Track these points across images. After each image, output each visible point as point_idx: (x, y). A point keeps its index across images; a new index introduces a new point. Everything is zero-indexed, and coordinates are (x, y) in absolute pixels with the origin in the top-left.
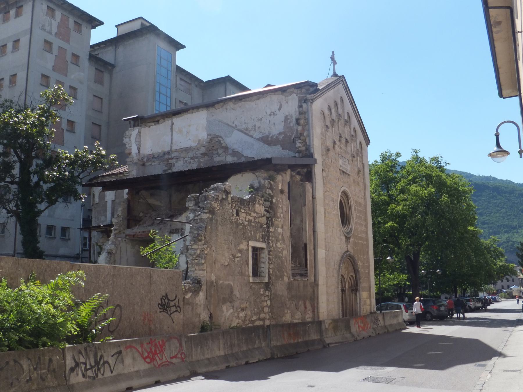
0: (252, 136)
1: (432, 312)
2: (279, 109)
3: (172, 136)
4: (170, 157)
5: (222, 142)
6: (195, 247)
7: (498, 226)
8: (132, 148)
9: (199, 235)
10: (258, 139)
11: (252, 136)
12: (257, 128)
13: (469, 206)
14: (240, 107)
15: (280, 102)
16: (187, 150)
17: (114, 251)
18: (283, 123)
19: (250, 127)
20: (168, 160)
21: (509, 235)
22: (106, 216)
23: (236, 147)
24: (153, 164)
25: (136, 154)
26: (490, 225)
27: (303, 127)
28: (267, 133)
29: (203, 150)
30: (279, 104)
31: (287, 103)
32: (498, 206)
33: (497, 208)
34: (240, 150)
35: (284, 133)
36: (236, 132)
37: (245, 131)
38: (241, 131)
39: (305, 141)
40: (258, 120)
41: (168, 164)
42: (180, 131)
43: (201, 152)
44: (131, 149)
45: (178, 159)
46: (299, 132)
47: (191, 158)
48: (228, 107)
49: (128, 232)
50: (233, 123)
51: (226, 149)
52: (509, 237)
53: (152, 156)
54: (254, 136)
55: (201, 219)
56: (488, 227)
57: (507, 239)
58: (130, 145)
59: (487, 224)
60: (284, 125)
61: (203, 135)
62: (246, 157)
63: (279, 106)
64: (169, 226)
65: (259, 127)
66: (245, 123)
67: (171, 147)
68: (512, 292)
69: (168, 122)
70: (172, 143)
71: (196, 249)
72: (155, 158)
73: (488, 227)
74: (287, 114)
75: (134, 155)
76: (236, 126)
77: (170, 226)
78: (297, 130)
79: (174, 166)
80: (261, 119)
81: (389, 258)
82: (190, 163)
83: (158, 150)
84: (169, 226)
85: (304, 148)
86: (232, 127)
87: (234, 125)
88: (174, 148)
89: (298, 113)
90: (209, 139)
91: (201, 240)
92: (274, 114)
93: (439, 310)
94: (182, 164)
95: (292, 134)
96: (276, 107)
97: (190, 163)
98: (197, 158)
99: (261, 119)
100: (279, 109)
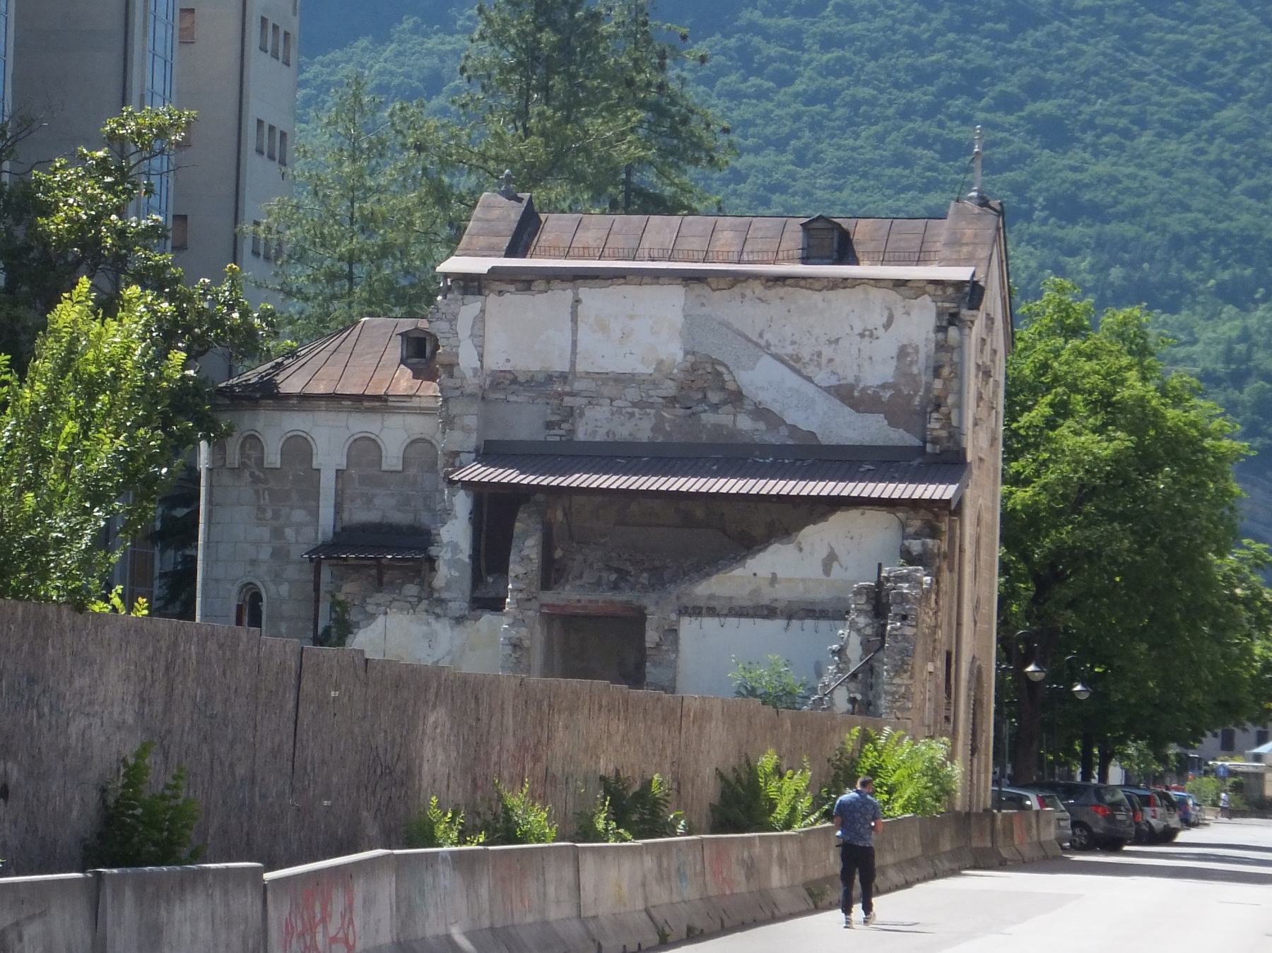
0: (809, 379)
1: (1090, 823)
2: (887, 326)
3: (575, 331)
4: (567, 389)
5: (727, 377)
6: (897, 681)
7: (1177, 242)
8: (461, 351)
9: (904, 662)
10: (828, 389)
11: (809, 379)
12: (824, 361)
13: (1225, 492)
14: (781, 298)
15: (889, 309)
16: (623, 380)
17: (526, 643)
18: (894, 363)
19: (806, 355)
20: (560, 396)
21: (1253, 320)
22: (315, 513)
23: (766, 398)
24: (512, 398)
25: (475, 370)
26: (1114, 229)
27: (944, 384)
28: (851, 379)
29: (670, 389)
30: (886, 313)
31: (908, 314)
32: (1197, 79)
33: (1185, 92)
34: (776, 408)
35: (893, 386)
36: (766, 361)
37: (791, 363)
38: (783, 361)
39: (948, 416)
40: (830, 342)
41: (560, 407)
42: (602, 326)
43: (664, 394)
44: (457, 355)
45: (592, 400)
46: (936, 393)
47: (634, 405)
48: (748, 293)
49: (549, 597)
50: (761, 336)
51: (736, 397)
52: (1245, 336)
53: (509, 376)
54: (816, 380)
55: (903, 635)
56: (1100, 244)
57: (1228, 357)
58: (453, 341)
59: (1097, 213)
60: (897, 368)
61: (673, 351)
62: (793, 429)
63: (885, 320)
64: (673, 597)
65: (831, 360)
66: (793, 343)
67: (573, 364)
68: (1259, 776)
69: (564, 295)
70: (574, 352)
71: (900, 686)
72: (521, 384)
73: (1100, 244)
74: (905, 342)
75: (469, 374)
76: (768, 345)
77: (678, 598)
78: (929, 388)
79: (582, 414)
80: (837, 340)
81: (1078, 688)
82: (632, 415)
83: (527, 363)
84: (673, 597)
85: (944, 433)
86: (756, 344)
87: (763, 343)
88: (580, 368)
89: (933, 345)
90: (689, 365)
91: (905, 672)
92: (871, 335)
93: (1111, 819)
94: (608, 415)
95: (916, 394)
96: (877, 319)
97: (632, 415)
98: (652, 405)
99: (837, 340)
100: (887, 326)
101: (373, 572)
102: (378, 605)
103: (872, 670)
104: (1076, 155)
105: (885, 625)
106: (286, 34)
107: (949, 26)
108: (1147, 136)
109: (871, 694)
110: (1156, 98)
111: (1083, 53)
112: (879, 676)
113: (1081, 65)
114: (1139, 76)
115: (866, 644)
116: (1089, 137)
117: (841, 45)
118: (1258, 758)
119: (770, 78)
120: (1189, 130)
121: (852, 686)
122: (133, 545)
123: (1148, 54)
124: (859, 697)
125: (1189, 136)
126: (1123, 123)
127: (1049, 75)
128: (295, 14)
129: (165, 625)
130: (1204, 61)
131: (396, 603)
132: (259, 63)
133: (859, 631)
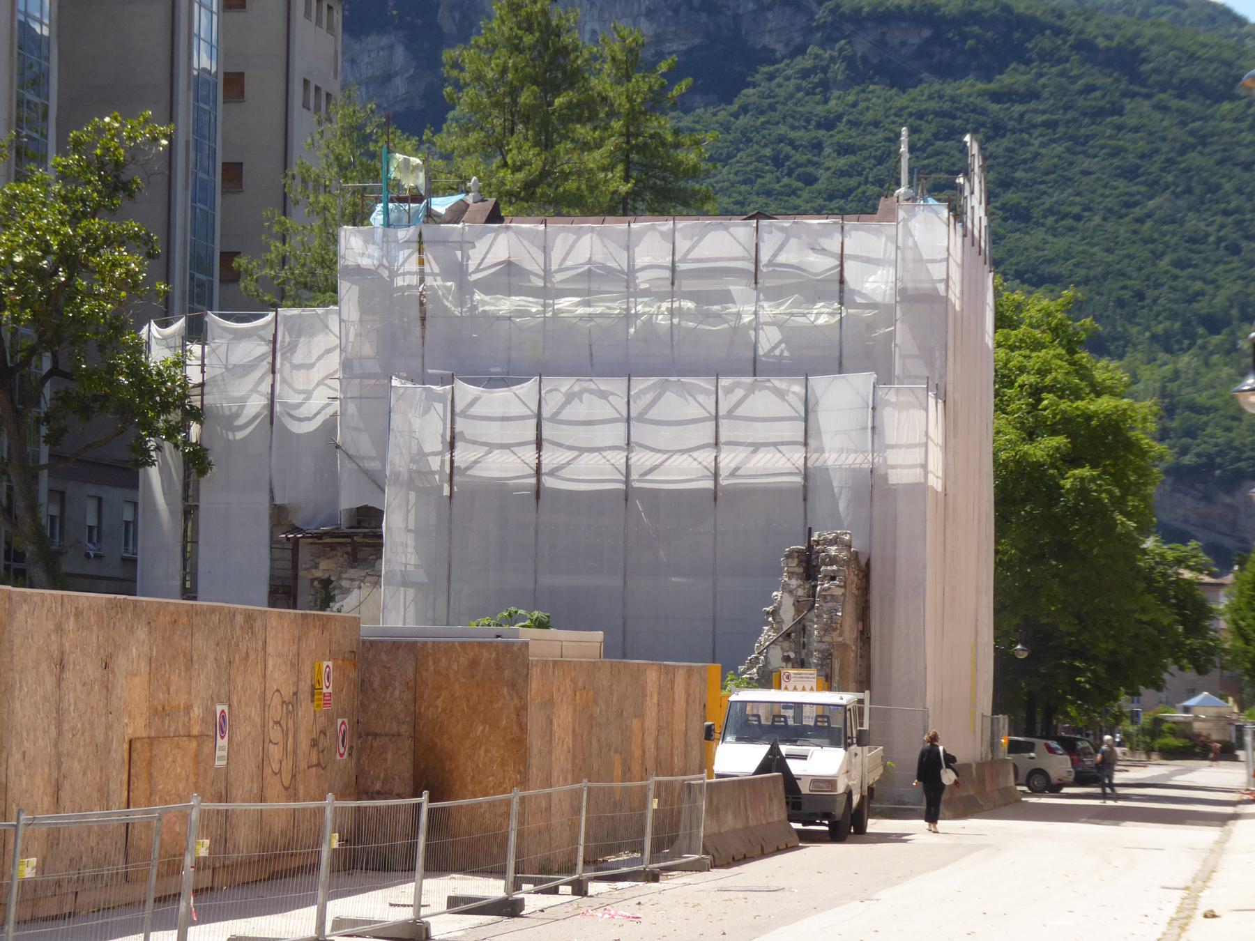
33: (1121, 184)
91: (835, 630)
101: (349, 549)
102: (352, 580)
103: (804, 629)
104: (1040, 235)
105: (815, 586)
106: (328, 95)
107: (936, 136)
108: (1097, 220)
109: (804, 652)
110: (1101, 191)
111: (1043, 156)
112: (811, 634)
113: (1041, 165)
114: (1086, 173)
115: (797, 603)
116: (1050, 220)
117: (853, 153)
118: (1187, 710)
119: (799, 179)
120: (1127, 215)
121: (786, 644)
122: (1102, 733)
123: (1095, 156)
124: (792, 655)
125: (1127, 219)
126: (1076, 210)
127: (1018, 175)
128: (336, 77)
129: (1036, 749)
130: (1138, 161)
131: (369, 578)
132: (303, 120)
133: (791, 592)
